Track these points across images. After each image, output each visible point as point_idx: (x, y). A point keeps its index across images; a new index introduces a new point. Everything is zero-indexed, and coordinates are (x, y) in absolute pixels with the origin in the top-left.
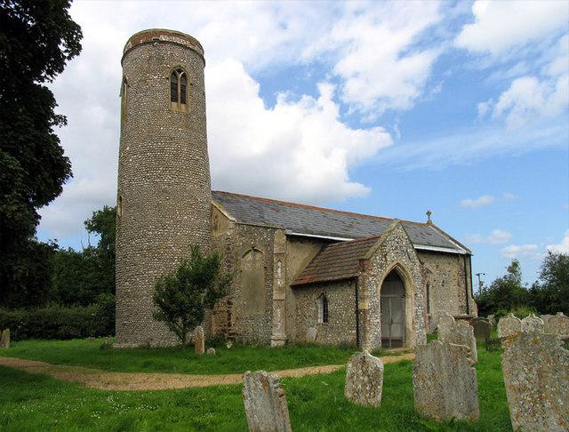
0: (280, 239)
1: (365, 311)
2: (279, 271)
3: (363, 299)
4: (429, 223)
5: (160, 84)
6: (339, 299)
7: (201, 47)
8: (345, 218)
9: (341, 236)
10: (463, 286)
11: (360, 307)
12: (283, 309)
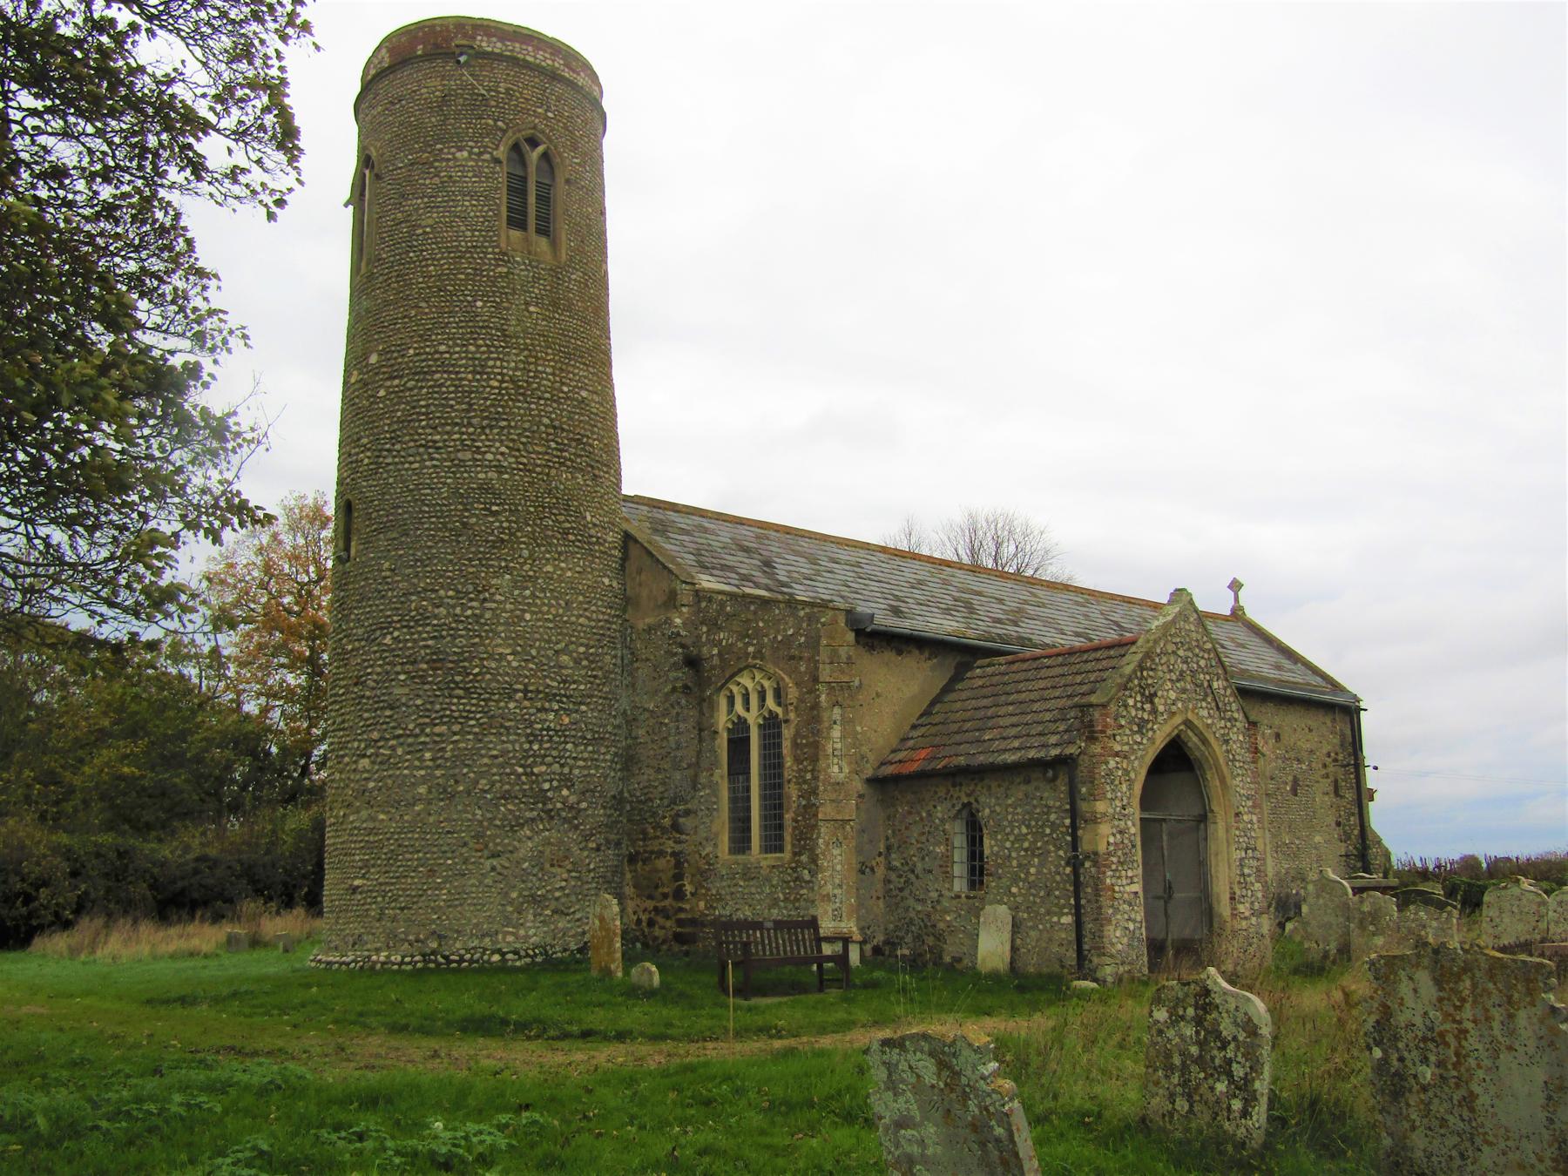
1: (1094, 856)
5: (475, 169)
7: (594, 77)
10: (1350, 795)
11: (1085, 846)
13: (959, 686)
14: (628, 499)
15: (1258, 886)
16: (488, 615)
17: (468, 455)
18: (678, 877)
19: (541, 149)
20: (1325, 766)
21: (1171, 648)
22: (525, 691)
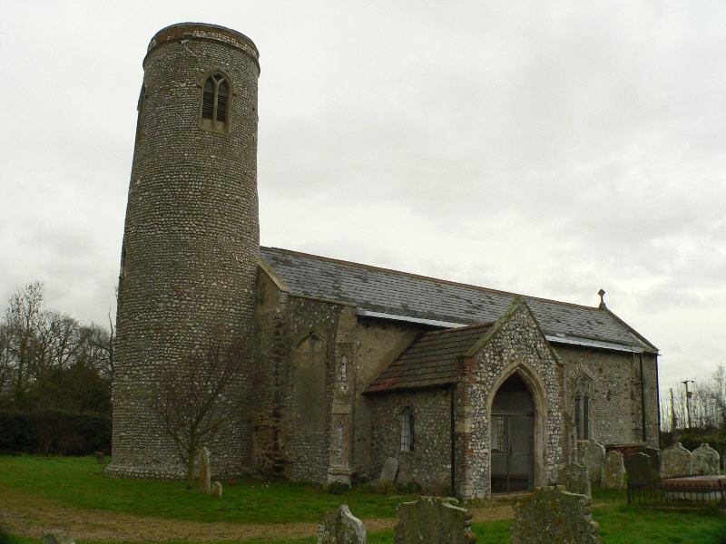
0: (346, 320)
1: (464, 436)
2: (344, 370)
3: (462, 417)
4: (602, 306)
5: (188, 92)
6: (429, 413)
7: (254, 48)
8: (466, 294)
9: (437, 318)
10: (639, 399)
11: (457, 430)
12: (408, 419)
13: (417, 345)
14: (262, 248)
15: (560, 449)
16: (183, 307)
17: (177, 228)
18: (276, 439)
19: (222, 80)
20: (626, 385)
21: (511, 327)
22: (200, 345)
